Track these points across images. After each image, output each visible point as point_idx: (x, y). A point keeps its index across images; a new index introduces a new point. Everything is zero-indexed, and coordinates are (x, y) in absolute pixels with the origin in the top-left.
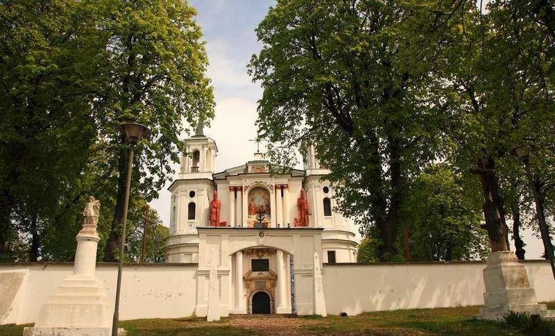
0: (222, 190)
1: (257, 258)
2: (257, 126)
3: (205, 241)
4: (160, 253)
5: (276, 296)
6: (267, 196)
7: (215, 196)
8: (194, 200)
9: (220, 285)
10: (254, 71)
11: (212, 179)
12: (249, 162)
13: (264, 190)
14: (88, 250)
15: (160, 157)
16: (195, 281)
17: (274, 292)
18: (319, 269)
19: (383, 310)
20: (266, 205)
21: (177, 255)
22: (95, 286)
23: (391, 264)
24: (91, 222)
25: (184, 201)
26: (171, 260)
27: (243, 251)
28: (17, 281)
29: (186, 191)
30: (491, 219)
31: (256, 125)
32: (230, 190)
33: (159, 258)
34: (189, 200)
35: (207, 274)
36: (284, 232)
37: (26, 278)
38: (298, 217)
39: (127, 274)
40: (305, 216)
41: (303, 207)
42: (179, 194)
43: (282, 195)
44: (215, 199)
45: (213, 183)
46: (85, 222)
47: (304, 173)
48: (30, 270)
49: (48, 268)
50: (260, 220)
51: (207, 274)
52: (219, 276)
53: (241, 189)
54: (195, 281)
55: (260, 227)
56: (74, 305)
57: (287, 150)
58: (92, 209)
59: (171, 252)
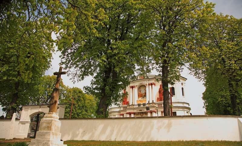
13: (144, 86)
19: (71, 140)
32: (131, 88)
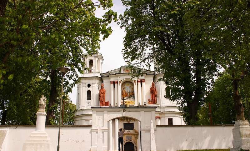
0: (106, 82)
1: (127, 122)
2: (123, 53)
3: (96, 114)
4: (71, 120)
5: (138, 144)
6: (132, 87)
7: (102, 87)
8: (90, 89)
9: (103, 136)
10: (121, 23)
11: (100, 76)
12: (122, 67)
14: (42, 119)
15: (73, 70)
16: (91, 134)
17: (137, 142)
18: (153, 128)
20: (132, 92)
21: (81, 121)
22: (45, 136)
23: (193, 126)
24: (42, 107)
25: (84, 90)
26: (77, 123)
27: (118, 118)
28: (4, 135)
29: (85, 84)
30: (237, 104)
31: (122, 51)
32: (111, 83)
33: (70, 123)
34: (87, 89)
35: (96, 131)
36: (136, 109)
37: (8, 133)
38: (151, 99)
39: (64, 131)
40: (154, 98)
41: (153, 93)
42: (82, 85)
43: (141, 86)
44: (102, 89)
45: (101, 79)
46: (40, 107)
47: (154, 72)
48: (9, 129)
49: (18, 128)
50: (124, 103)
51: (96, 131)
52: (103, 132)
53: (117, 82)
54: (91, 134)
55: (124, 107)
56: (37, 144)
57: (139, 65)
58: (43, 101)
59: (77, 119)
